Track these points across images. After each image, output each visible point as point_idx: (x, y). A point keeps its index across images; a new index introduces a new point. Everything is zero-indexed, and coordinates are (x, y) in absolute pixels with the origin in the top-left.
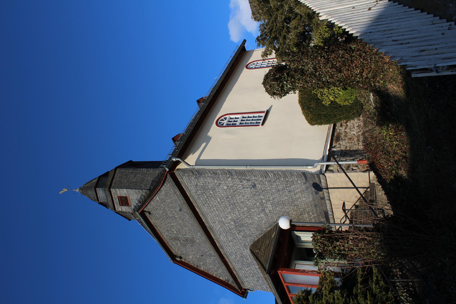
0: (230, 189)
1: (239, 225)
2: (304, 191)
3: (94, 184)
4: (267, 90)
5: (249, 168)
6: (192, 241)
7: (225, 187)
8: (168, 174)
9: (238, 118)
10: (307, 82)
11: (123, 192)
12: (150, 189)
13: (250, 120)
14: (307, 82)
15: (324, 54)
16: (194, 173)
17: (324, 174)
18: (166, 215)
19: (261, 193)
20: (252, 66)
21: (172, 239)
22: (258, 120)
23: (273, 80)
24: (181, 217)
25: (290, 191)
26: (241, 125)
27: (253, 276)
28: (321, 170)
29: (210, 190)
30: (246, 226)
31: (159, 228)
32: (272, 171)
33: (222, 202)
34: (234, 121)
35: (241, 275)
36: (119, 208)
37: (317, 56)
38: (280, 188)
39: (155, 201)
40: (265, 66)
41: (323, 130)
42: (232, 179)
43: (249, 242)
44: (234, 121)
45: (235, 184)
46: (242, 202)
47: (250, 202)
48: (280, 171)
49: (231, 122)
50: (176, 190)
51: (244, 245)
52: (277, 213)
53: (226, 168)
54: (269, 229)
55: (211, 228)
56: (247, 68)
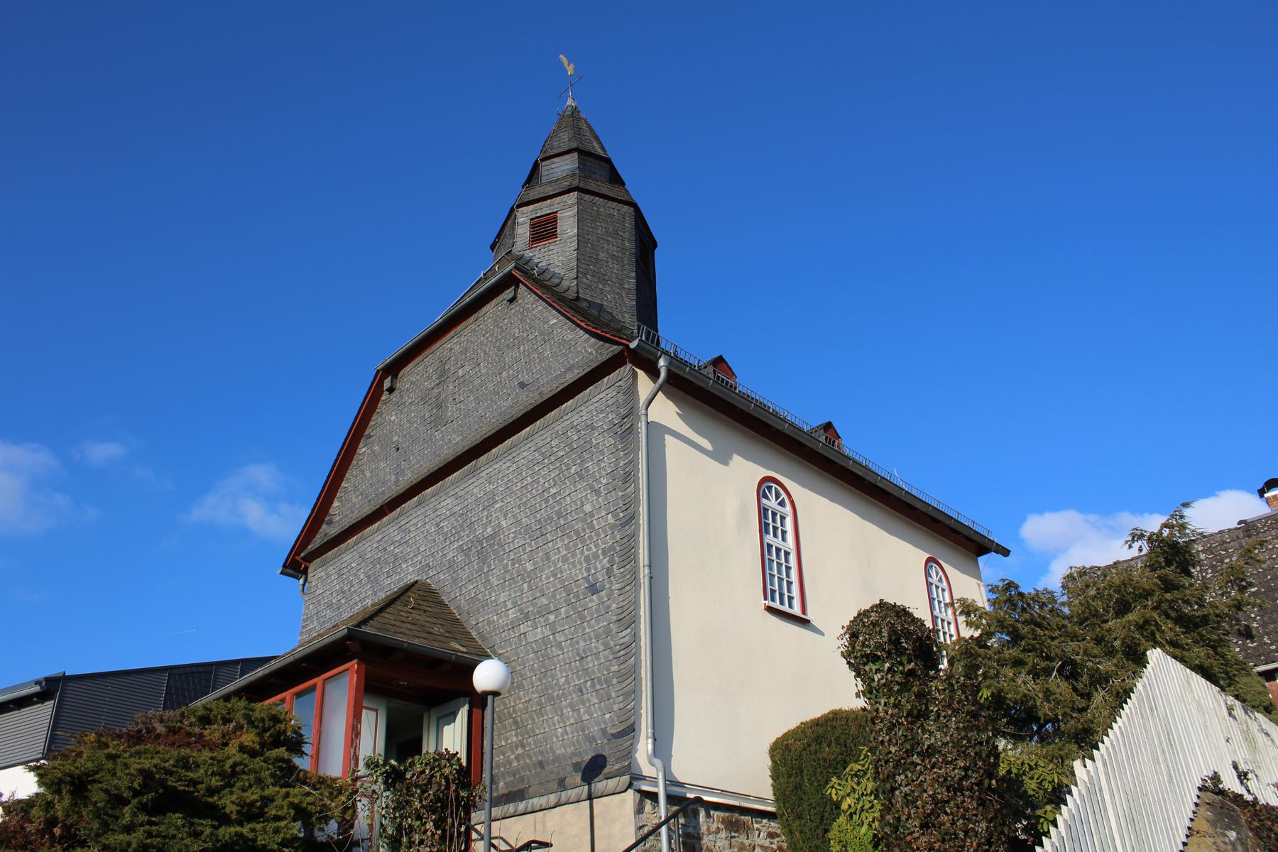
0: (584, 520)
1: (483, 550)
2: (583, 730)
3: (588, 148)
4: (862, 615)
5: (644, 573)
6: (438, 421)
7: (588, 508)
8: (621, 348)
9: (784, 539)
10: (890, 729)
11: (568, 226)
12: (578, 298)
13: (779, 572)
14: (890, 729)
15: (974, 778)
16: (626, 424)
17: (630, 785)
19: (573, 609)
20: (934, 574)
22: (781, 595)
23: (893, 631)
24: (504, 387)
25: (580, 690)
26: (765, 548)
28: (643, 778)
30: (481, 569)
31: (473, 326)
32: (635, 637)
33: (547, 501)
34: (775, 529)
37: (966, 755)
38: (591, 663)
39: (546, 314)
40: (937, 612)
41: (754, 781)
42: (613, 527)
43: (438, 579)
44: (775, 529)
45: (598, 535)
46: (547, 556)
47: (548, 578)
48: (638, 661)
49: (774, 521)
50: (576, 371)
52: (517, 654)
54: (474, 634)
55: (473, 472)
56: (929, 560)
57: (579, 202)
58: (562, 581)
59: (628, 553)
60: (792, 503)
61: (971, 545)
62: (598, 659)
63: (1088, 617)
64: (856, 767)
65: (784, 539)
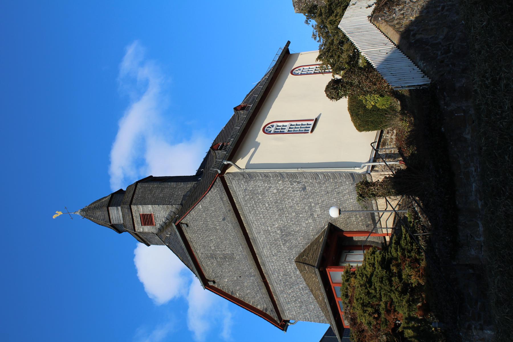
0: (279, 193)
1: (286, 234)
2: (352, 192)
3: (107, 203)
4: (327, 96)
5: (300, 170)
6: (231, 257)
7: (275, 191)
8: (218, 178)
9: (286, 126)
10: (354, 91)
11: (148, 209)
12: (181, 204)
13: (298, 128)
14: (354, 91)
15: (365, 73)
16: (246, 176)
17: (369, 174)
18: (206, 226)
19: (310, 196)
20: (297, 72)
21: (207, 257)
22: (306, 127)
23: (332, 89)
24: (223, 227)
25: (338, 193)
26: (289, 132)
27: (296, 300)
28: (367, 171)
29: (259, 194)
30: (293, 235)
31: (194, 243)
32: (322, 173)
33: (270, 208)
34: (282, 129)
35: (282, 300)
36: (140, 228)
37: (360, 75)
38: (329, 189)
39: (196, 210)
40: (312, 72)
41: (372, 136)
42: (283, 181)
43: (294, 254)
44: (282, 129)
45: (285, 187)
46: (291, 207)
47: (299, 207)
48: (329, 172)
49: (279, 129)
50: (224, 195)
51: (289, 259)
52: (325, 218)
53: (278, 171)
54: (317, 237)
55: (254, 240)
56: (292, 73)
57: (135, 204)
58: (300, 201)
59: (293, 176)
60: (270, 123)
61: (286, 57)
62: (328, 187)
63: (327, 36)
64: (364, 101)
65: (286, 126)
